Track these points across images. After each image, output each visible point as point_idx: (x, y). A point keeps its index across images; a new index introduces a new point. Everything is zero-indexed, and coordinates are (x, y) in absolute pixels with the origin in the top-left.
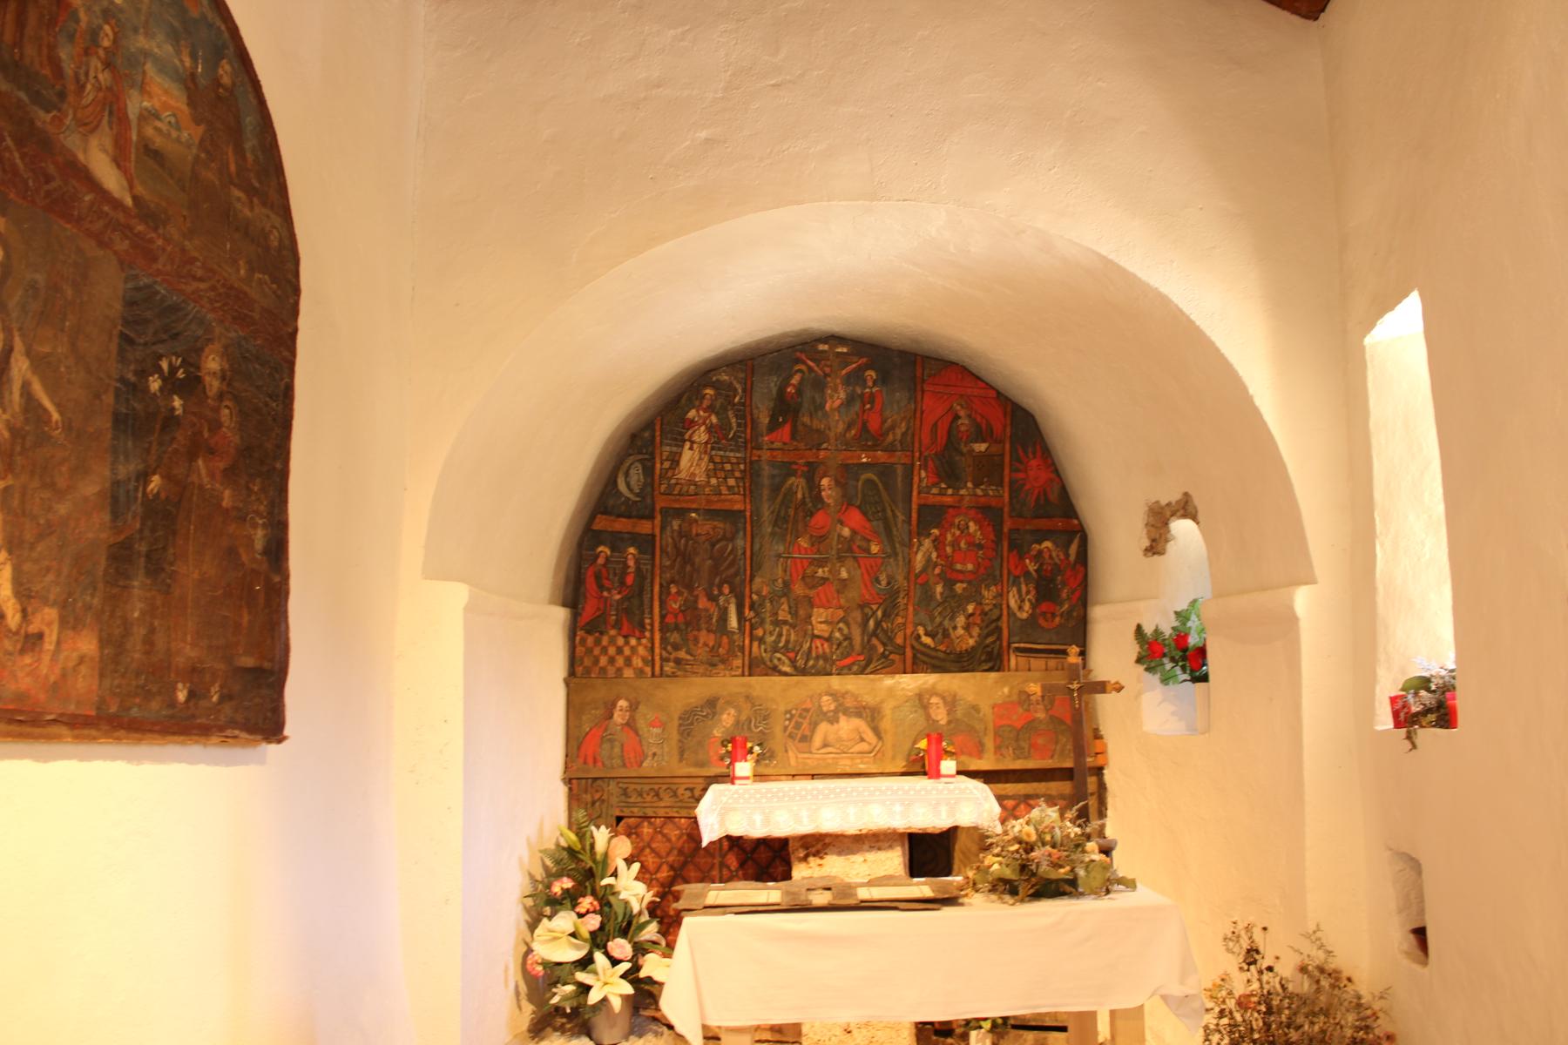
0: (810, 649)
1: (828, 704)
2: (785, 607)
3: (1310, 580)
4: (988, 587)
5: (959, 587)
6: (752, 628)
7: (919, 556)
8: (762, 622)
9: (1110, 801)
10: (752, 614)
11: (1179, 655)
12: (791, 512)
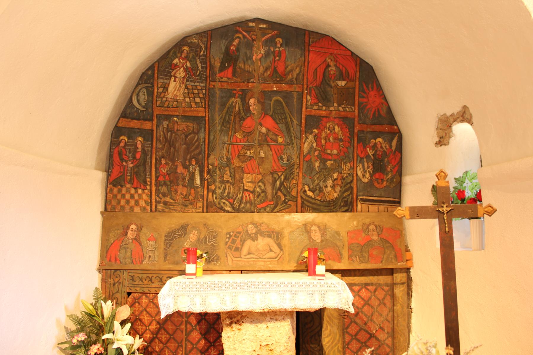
0: (242, 197)
2: (228, 172)
4: (345, 164)
5: (329, 163)
6: (209, 184)
8: (214, 181)
9: (414, 287)
10: (209, 177)
12: (232, 118)
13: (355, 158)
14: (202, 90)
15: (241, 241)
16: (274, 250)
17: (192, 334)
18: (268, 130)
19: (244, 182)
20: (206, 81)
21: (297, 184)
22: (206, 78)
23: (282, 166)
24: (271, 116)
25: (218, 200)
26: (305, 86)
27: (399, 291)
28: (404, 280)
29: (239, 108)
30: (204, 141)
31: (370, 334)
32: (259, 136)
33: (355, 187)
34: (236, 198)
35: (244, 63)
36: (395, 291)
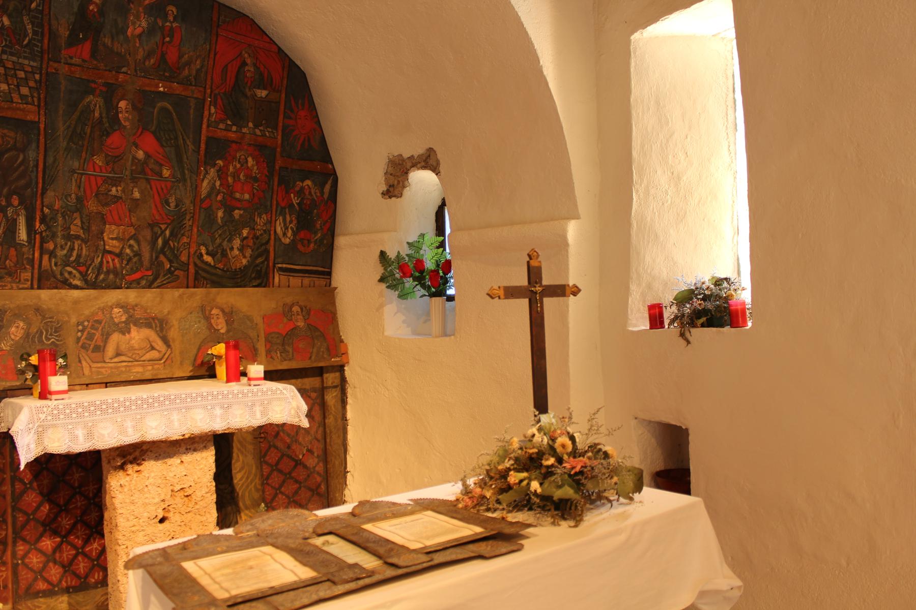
0: (101, 263)
1: (118, 315)
2: (78, 222)
3: (577, 217)
4: (260, 216)
5: (237, 213)
6: (43, 241)
7: (205, 184)
8: (54, 236)
9: (349, 391)
10: (43, 227)
11: (423, 277)
12: (88, 130)
13: (274, 207)
14: (33, 73)
15: (102, 335)
16: (158, 348)
17: (25, 497)
18: (148, 155)
19: (106, 238)
20: (42, 58)
21: (189, 244)
22: (42, 52)
23: (167, 215)
24: (154, 133)
25: (60, 268)
26: (209, 91)
27: (331, 398)
28: (337, 382)
29: (101, 114)
30: (37, 166)
31: (296, 461)
32: (132, 165)
33: (271, 249)
34: (90, 265)
35: (113, 39)
36: (326, 397)
